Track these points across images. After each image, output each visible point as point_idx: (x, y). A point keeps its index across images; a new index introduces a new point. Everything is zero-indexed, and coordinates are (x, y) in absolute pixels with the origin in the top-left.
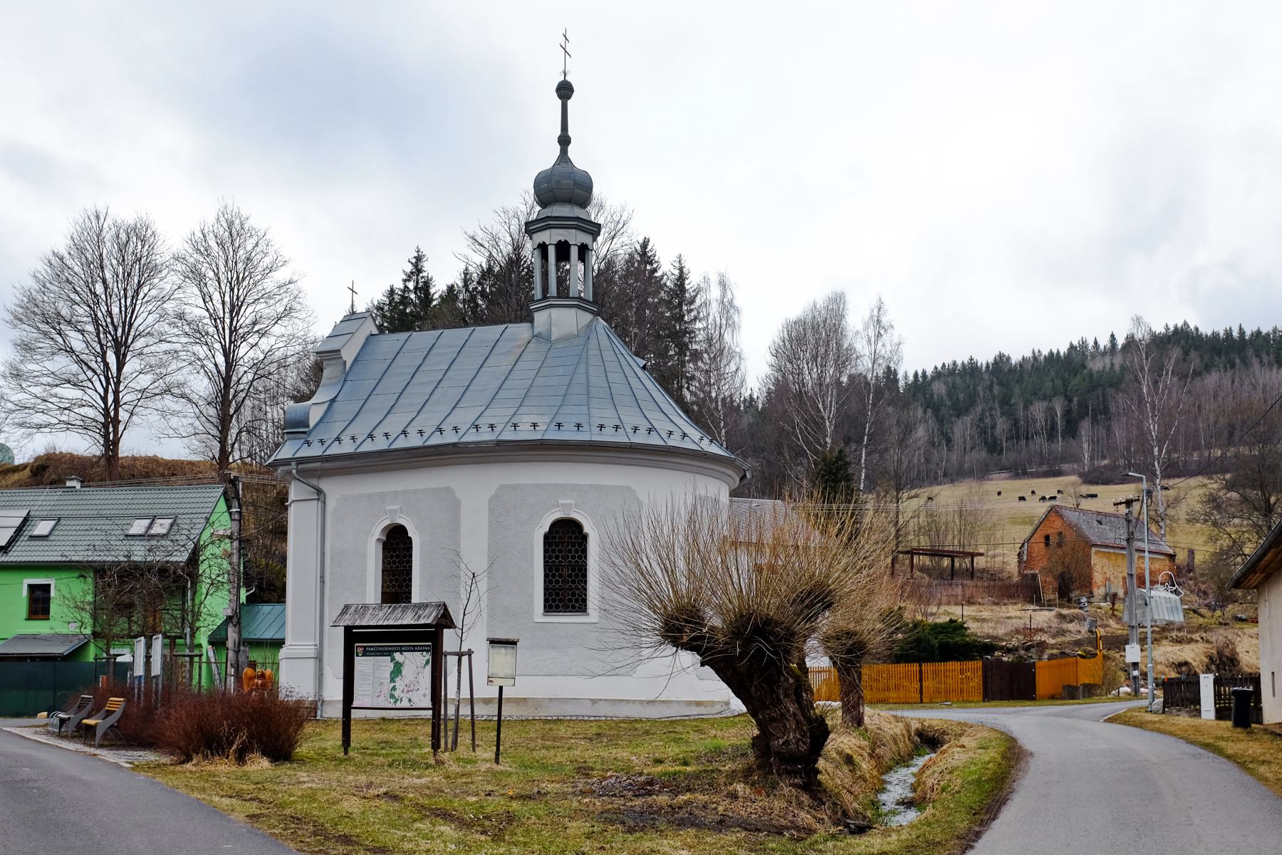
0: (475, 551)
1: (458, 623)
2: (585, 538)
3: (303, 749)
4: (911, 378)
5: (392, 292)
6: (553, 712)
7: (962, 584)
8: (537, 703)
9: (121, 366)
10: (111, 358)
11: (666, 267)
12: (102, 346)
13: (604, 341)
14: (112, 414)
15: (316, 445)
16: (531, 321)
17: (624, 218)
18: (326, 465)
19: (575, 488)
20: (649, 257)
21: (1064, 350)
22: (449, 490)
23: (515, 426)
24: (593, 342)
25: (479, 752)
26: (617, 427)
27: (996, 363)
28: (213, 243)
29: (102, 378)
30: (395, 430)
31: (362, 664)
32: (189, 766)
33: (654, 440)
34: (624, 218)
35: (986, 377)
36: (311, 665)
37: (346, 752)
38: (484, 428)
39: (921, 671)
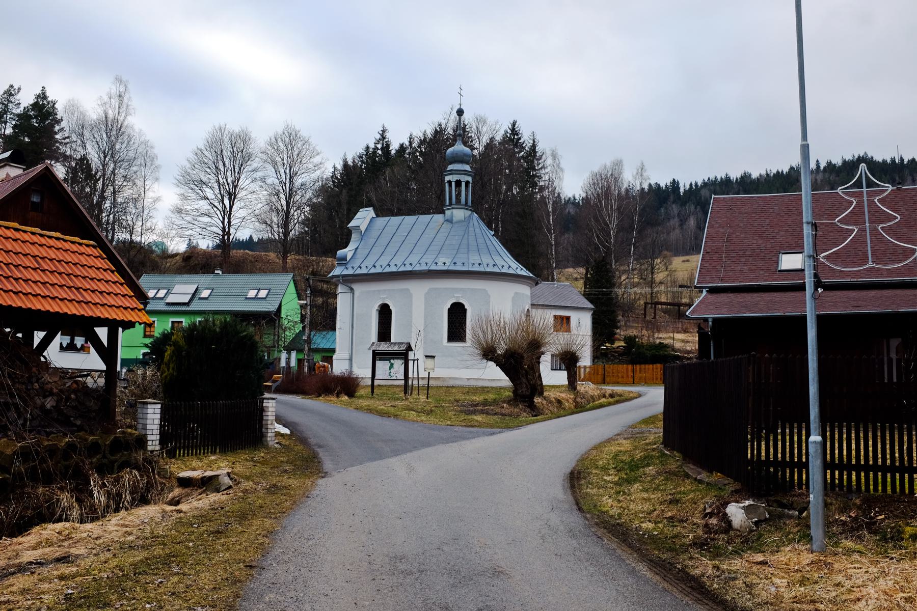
0: (418, 321)
1: (414, 349)
2: (465, 310)
3: (357, 394)
4: (688, 187)
5: (368, 147)
6: (451, 383)
7: (682, 322)
8: (444, 379)
9: (231, 207)
10: (226, 202)
11: (526, 138)
12: (221, 195)
13: (476, 224)
14: (227, 230)
15: (350, 269)
16: (444, 213)
17: (497, 128)
18: (355, 278)
19: (461, 289)
20: (516, 131)
21: (786, 170)
22: (408, 290)
23: (436, 263)
24: (471, 224)
25: (420, 396)
26: (480, 264)
27: (742, 177)
28: (280, 144)
29: (222, 213)
30: (385, 264)
31: (379, 364)
32: (321, 398)
33: (496, 270)
34: (497, 128)
35: (735, 186)
36: (347, 362)
37: (372, 395)
38: (423, 264)
39: (633, 369)
